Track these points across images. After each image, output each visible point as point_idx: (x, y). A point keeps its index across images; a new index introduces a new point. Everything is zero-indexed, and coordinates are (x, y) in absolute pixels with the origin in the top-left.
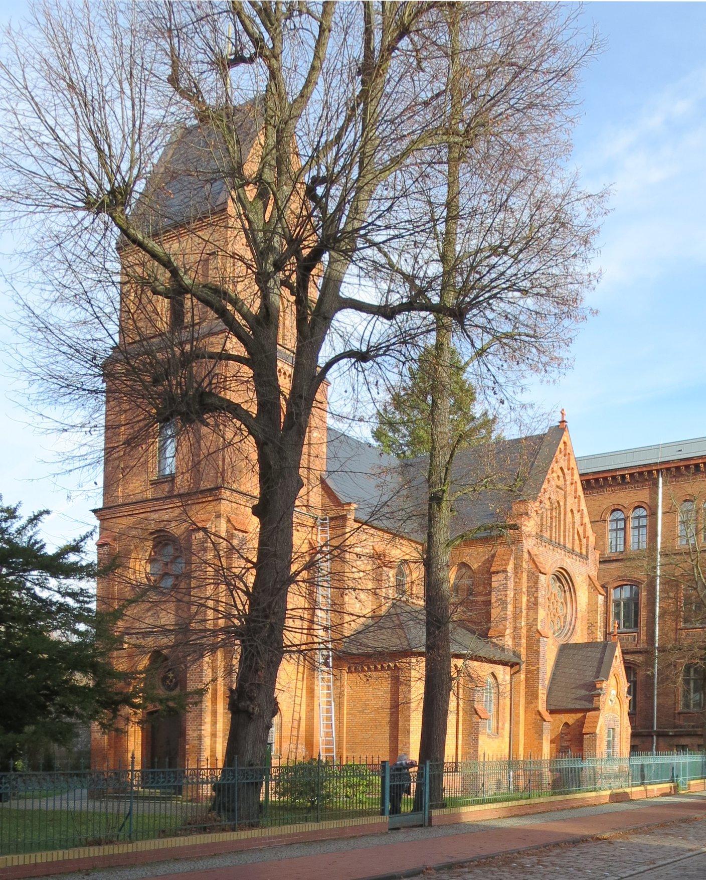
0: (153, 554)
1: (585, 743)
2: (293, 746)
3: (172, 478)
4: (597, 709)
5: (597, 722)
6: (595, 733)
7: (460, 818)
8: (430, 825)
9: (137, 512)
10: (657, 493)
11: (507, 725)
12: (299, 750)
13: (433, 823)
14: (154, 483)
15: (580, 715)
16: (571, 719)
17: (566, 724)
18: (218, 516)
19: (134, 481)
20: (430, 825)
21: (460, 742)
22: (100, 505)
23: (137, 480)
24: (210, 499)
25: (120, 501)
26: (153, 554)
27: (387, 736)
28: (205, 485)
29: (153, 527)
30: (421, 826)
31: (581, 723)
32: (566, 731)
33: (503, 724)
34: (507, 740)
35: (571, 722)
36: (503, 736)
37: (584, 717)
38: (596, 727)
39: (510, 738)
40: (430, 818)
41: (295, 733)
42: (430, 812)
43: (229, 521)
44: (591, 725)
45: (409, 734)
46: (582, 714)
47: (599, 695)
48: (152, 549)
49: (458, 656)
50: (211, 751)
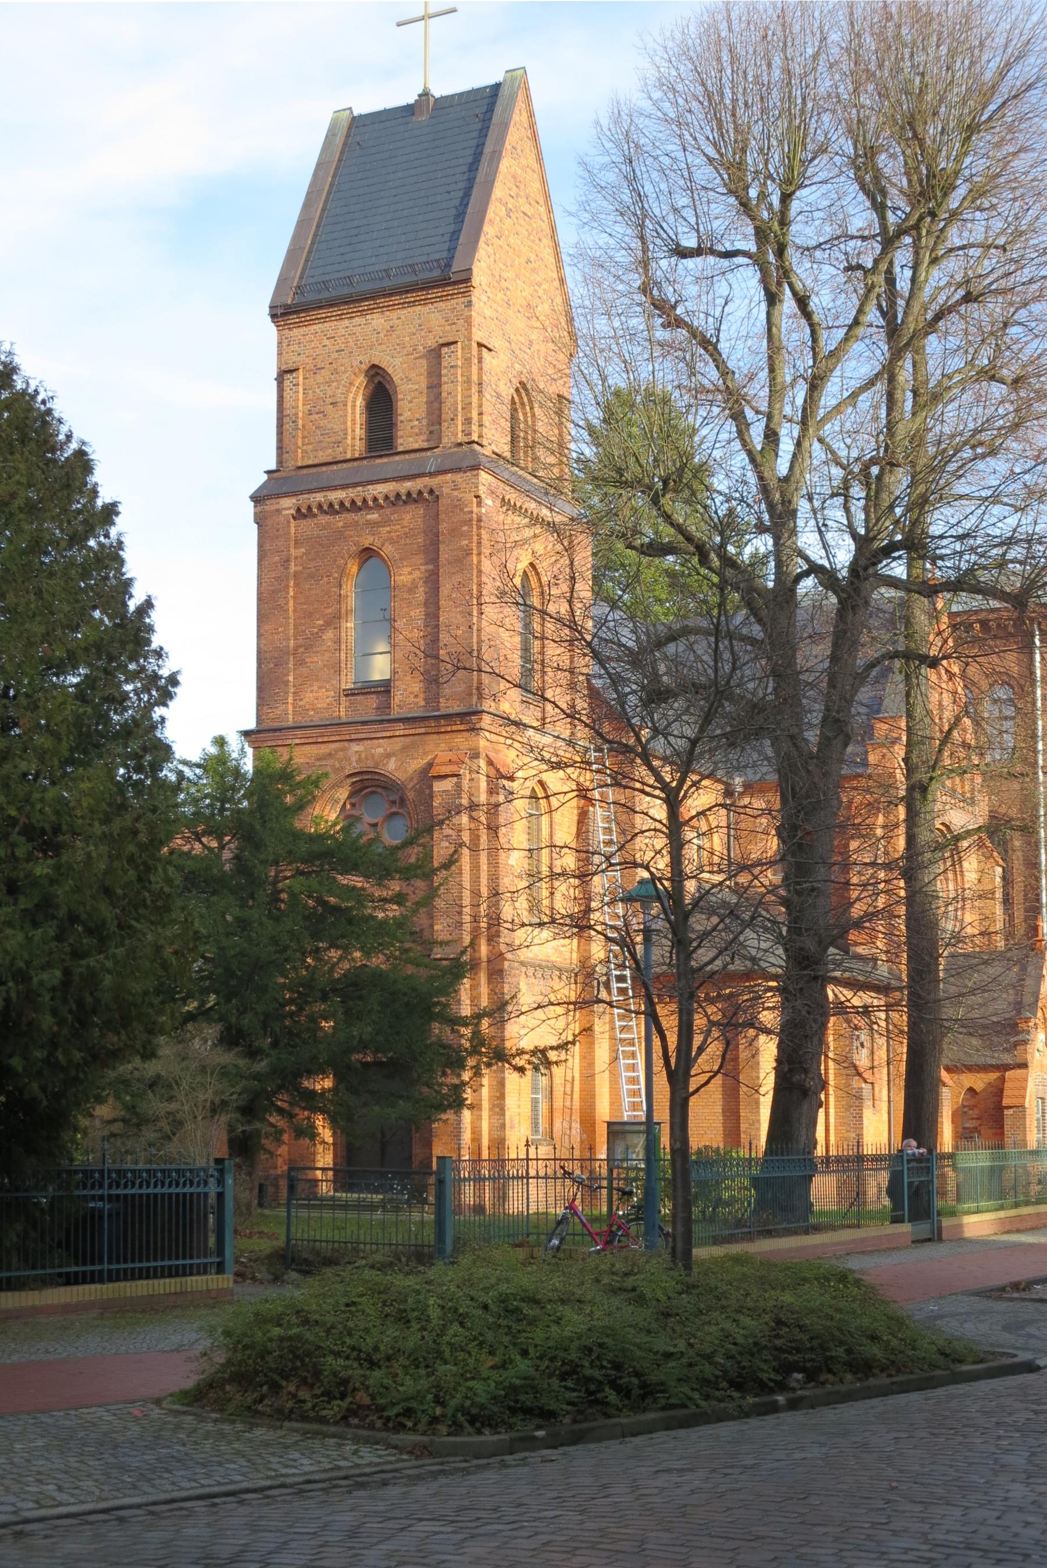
0: (348, 806)
1: (1008, 1122)
2: (566, 1125)
3: (384, 689)
4: (1024, 1066)
5: (1025, 1089)
6: (1023, 1106)
7: (962, 1232)
8: (940, 1239)
9: (326, 739)
10: (1032, 660)
11: (885, 1092)
12: (573, 1132)
13: (944, 1236)
14: (350, 694)
15: (993, 1076)
16: (979, 1081)
17: (971, 1090)
18: (476, 755)
19: (315, 688)
20: (940, 1239)
21: (832, 1120)
22: (251, 724)
23: (320, 688)
24: (460, 727)
25: (290, 722)
26: (348, 806)
27: (719, 1109)
28: (449, 705)
29: (354, 766)
30: (929, 1240)
31: (997, 1090)
32: (971, 1103)
33: (880, 1091)
34: (886, 1116)
35: (979, 1086)
36: (880, 1111)
37: (1003, 1079)
38: (1024, 1097)
39: (889, 1113)
40: (940, 1229)
41: (568, 1104)
42: (939, 1222)
43: (490, 763)
44: (1016, 1093)
45: (758, 1108)
46: (997, 1074)
47: (1025, 1042)
48: (349, 797)
49: (837, 982)
50: (473, 1133)
